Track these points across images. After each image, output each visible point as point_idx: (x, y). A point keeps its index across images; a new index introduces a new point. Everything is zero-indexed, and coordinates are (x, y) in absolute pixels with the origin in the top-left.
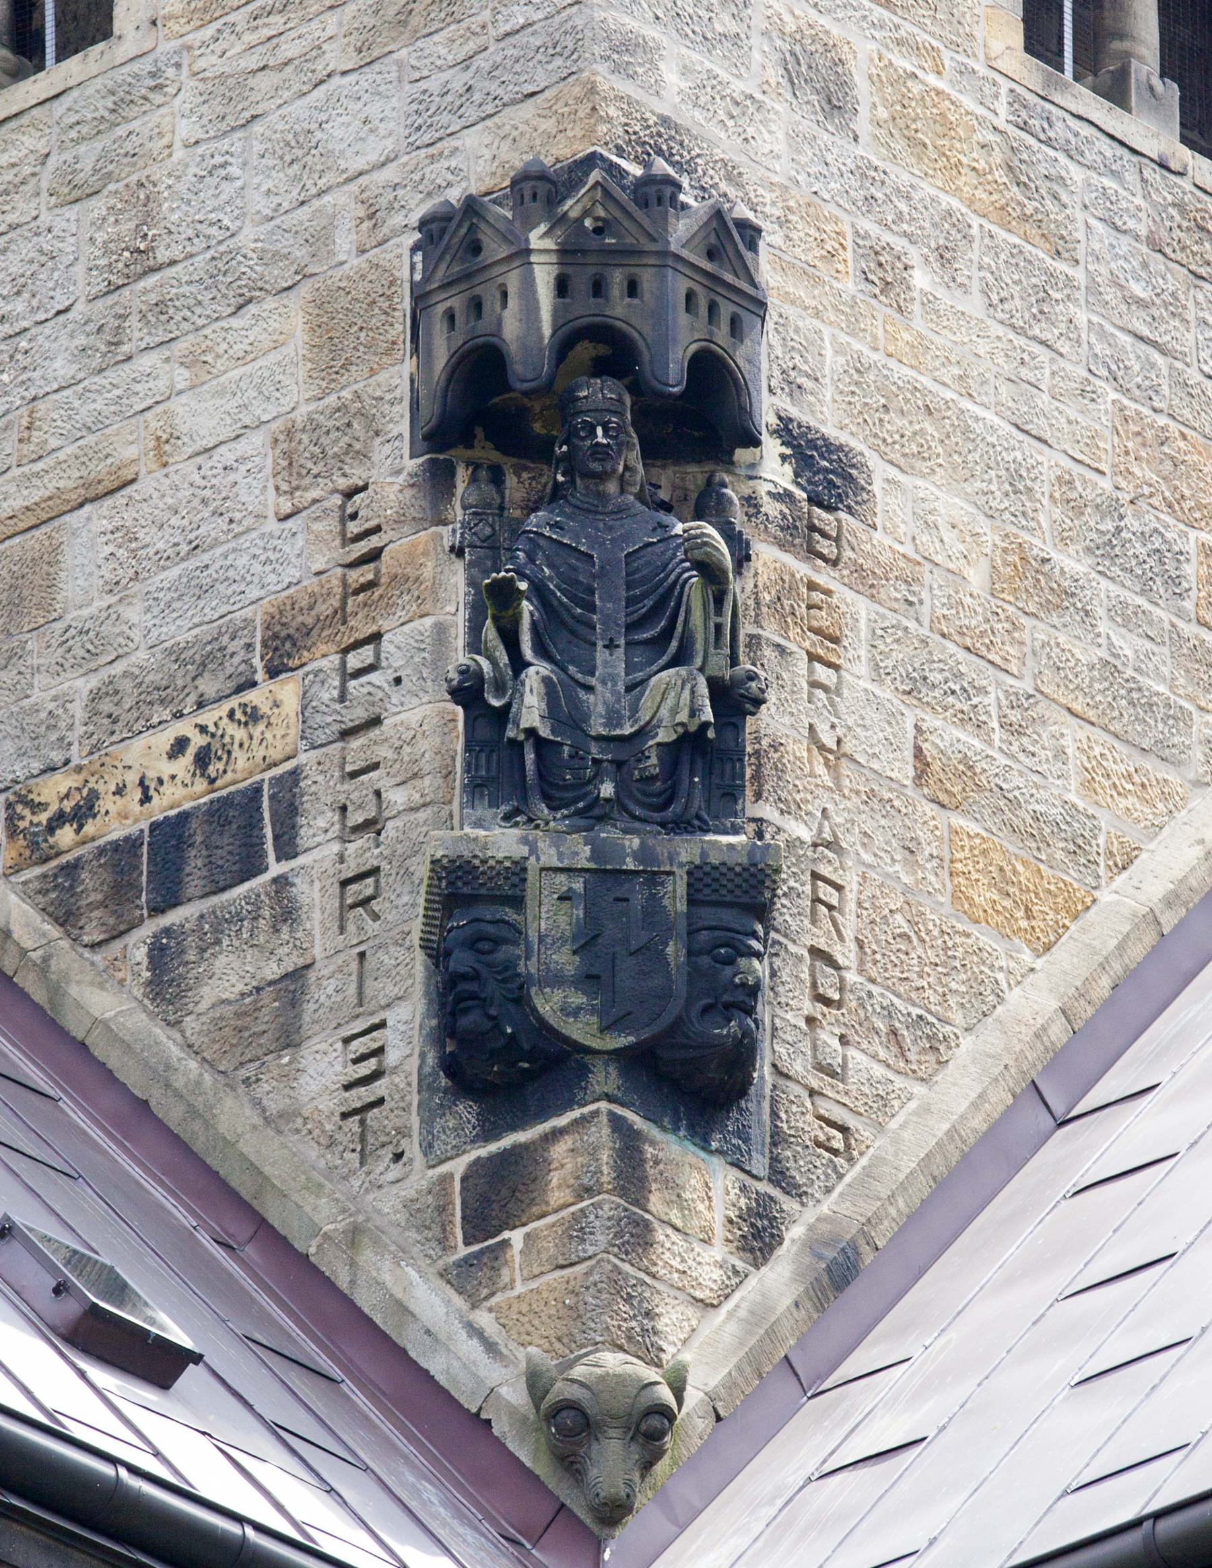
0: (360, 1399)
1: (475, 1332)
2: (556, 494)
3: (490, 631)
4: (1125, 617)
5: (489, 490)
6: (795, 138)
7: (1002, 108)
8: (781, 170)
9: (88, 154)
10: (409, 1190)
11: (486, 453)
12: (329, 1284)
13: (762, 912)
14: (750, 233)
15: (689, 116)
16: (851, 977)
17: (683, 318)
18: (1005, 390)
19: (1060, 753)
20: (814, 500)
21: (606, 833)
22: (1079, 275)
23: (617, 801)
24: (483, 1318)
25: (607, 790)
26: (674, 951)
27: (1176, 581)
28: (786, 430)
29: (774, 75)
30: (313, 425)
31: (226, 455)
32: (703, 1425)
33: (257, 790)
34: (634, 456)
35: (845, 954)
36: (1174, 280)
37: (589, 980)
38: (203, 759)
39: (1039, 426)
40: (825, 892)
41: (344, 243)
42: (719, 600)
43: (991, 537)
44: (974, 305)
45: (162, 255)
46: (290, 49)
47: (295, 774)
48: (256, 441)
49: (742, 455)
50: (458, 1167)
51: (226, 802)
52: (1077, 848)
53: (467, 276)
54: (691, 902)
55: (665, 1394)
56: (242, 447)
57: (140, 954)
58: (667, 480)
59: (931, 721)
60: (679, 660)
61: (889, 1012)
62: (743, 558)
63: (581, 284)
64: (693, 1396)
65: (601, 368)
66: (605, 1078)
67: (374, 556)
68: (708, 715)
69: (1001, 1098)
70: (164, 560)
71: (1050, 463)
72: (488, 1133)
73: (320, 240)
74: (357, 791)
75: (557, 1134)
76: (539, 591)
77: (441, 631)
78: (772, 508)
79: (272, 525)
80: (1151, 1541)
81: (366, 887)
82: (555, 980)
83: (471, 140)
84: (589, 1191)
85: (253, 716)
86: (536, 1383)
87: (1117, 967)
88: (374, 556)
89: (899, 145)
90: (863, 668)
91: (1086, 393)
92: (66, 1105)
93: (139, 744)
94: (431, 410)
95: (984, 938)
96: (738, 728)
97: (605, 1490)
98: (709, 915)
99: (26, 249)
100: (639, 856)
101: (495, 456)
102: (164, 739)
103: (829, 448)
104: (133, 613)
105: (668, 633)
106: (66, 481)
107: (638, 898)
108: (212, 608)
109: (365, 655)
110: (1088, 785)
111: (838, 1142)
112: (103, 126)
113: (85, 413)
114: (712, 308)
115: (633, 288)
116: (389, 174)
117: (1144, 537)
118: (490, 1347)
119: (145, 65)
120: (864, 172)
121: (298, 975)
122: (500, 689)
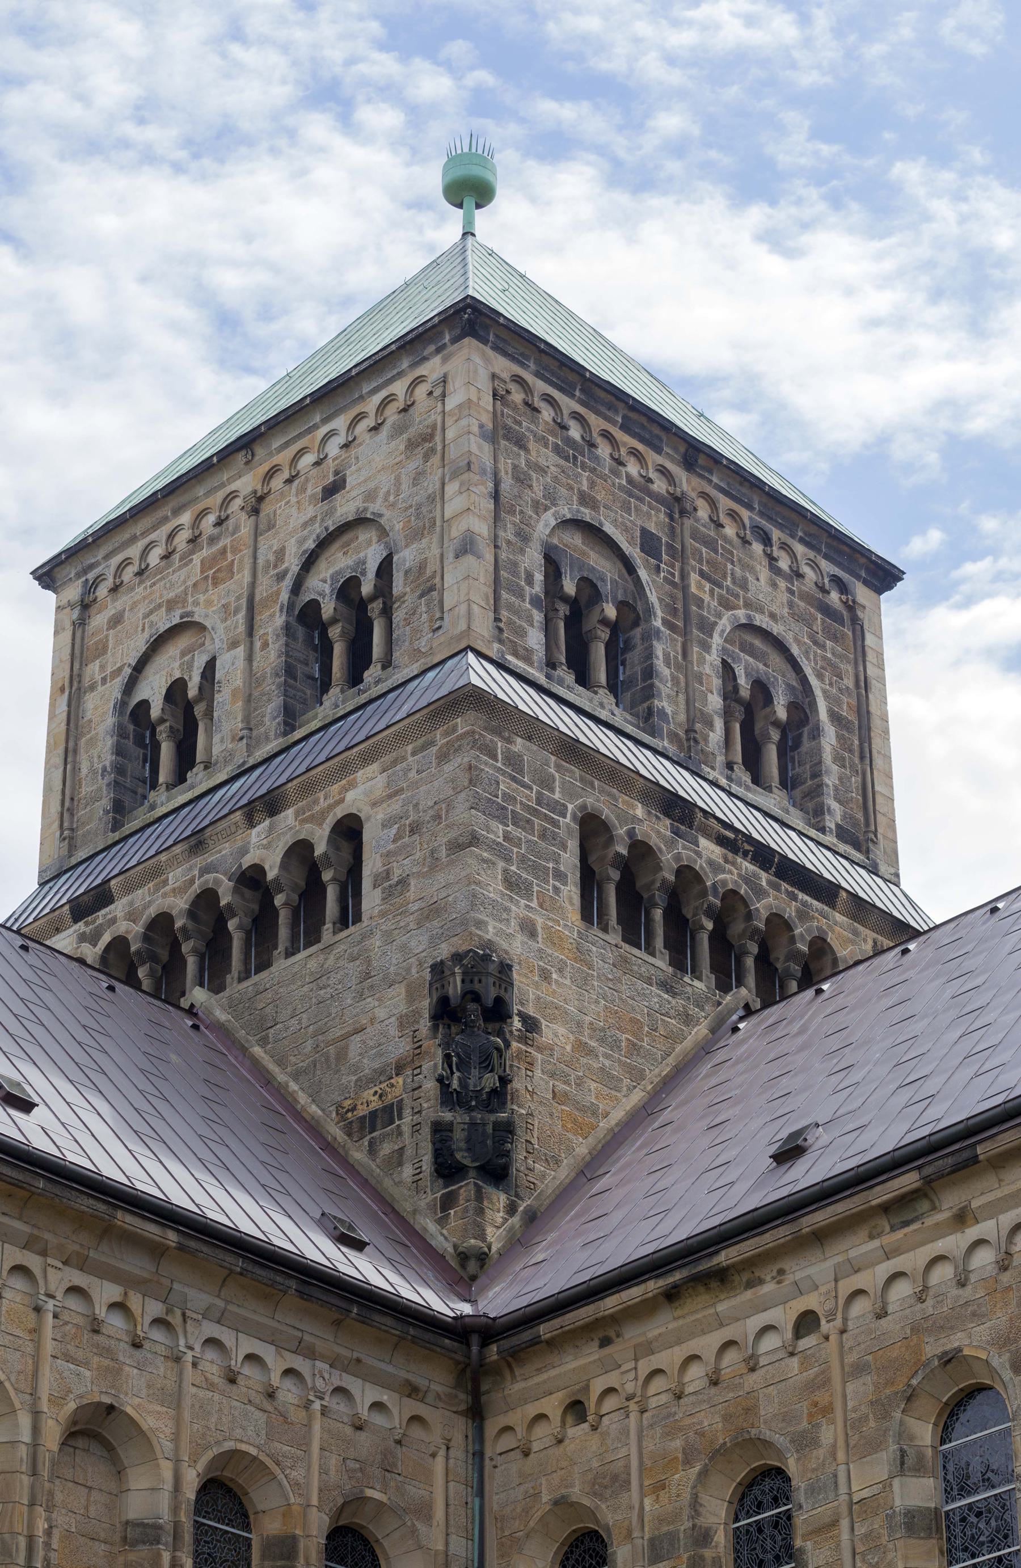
0: (415, 1251)
1: (442, 1235)
2: (463, 1031)
3: (446, 1065)
4: (607, 1056)
5: (447, 1031)
6: (523, 943)
7: (575, 934)
8: (519, 951)
9: (356, 949)
10: (427, 1200)
11: (447, 1021)
12: (409, 1223)
13: (512, 1132)
14: (510, 967)
15: (496, 939)
16: (536, 1146)
17: (492, 988)
18: (576, 1002)
19: (590, 1090)
20: (527, 1031)
21: (474, 1114)
22: (595, 974)
23: (476, 1106)
24: (445, 1232)
25: (473, 1103)
26: (489, 1142)
27: (619, 1047)
28: (520, 1014)
29: (518, 928)
30: (406, 1015)
31: (387, 1022)
32: (496, 1256)
33: (393, 1104)
34: (481, 1022)
35: (535, 1141)
36: (619, 973)
37: (469, 1150)
38: (381, 1096)
39: (585, 1010)
40: (529, 1126)
41: (414, 971)
42: (501, 1056)
43: (572, 1038)
44: (568, 982)
45: (372, 974)
46: (402, 924)
47: (402, 1100)
48: (393, 1019)
49: (509, 1020)
50: (439, 1195)
51: (386, 1107)
52: (594, 1113)
53: (441, 979)
54: (494, 1130)
55: (486, 1250)
56: (390, 1020)
57: (366, 1143)
58: (490, 1027)
59: (557, 1083)
60: (491, 1071)
61: (545, 1155)
62: (508, 1045)
63: (468, 980)
64: (494, 1249)
65: (474, 1000)
66: (472, 1173)
67: (420, 1046)
68: (498, 1084)
69: (573, 1174)
70: (372, 1048)
71: (588, 1019)
72: (446, 1187)
73: (408, 970)
74: (415, 1104)
75: (461, 1187)
76: (458, 1055)
77: (435, 1065)
78: (516, 1033)
79: (397, 1039)
80: (588, 1286)
81: (418, 1127)
82: (461, 1150)
83: (443, 946)
84: (468, 1201)
85: (392, 1086)
86: (455, 1247)
87: (603, 1142)
88: (420, 1046)
89: (549, 944)
90: (539, 1071)
91: (597, 1002)
92: (348, 1180)
93: (366, 1093)
94: (433, 1012)
95: (570, 1135)
96: (506, 1088)
97: (471, 1273)
98: (498, 1133)
99: (342, 973)
100: (481, 1119)
101: (449, 1022)
102: (372, 1091)
103: (530, 1017)
104: (365, 1061)
105: (489, 1065)
106: (350, 1029)
107: (480, 1130)
108: (383, 1059)
109: (418, 1070)
110: (597, 1097)
111: (532, 1186)
112: (360, 942)
113: (354, 1012)
114: (500, 985)
115: (480, 981)
116: (423, 954)
117: (611, 1037)
118: (446, 1238)
119: (369, 928)
120: (540, 950)
121: (402, 1148)
122: (448, 1079)
